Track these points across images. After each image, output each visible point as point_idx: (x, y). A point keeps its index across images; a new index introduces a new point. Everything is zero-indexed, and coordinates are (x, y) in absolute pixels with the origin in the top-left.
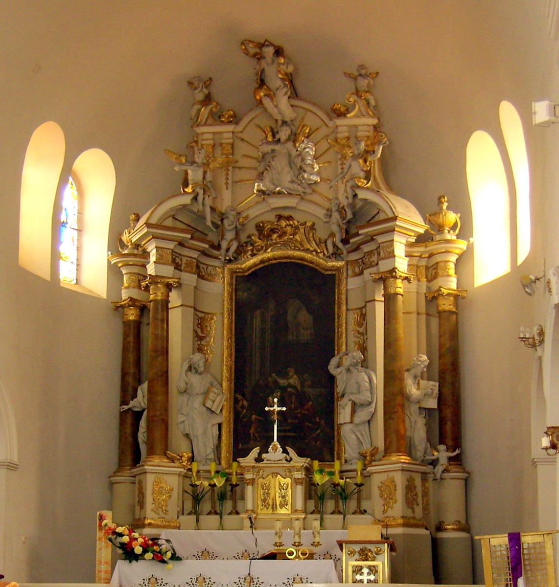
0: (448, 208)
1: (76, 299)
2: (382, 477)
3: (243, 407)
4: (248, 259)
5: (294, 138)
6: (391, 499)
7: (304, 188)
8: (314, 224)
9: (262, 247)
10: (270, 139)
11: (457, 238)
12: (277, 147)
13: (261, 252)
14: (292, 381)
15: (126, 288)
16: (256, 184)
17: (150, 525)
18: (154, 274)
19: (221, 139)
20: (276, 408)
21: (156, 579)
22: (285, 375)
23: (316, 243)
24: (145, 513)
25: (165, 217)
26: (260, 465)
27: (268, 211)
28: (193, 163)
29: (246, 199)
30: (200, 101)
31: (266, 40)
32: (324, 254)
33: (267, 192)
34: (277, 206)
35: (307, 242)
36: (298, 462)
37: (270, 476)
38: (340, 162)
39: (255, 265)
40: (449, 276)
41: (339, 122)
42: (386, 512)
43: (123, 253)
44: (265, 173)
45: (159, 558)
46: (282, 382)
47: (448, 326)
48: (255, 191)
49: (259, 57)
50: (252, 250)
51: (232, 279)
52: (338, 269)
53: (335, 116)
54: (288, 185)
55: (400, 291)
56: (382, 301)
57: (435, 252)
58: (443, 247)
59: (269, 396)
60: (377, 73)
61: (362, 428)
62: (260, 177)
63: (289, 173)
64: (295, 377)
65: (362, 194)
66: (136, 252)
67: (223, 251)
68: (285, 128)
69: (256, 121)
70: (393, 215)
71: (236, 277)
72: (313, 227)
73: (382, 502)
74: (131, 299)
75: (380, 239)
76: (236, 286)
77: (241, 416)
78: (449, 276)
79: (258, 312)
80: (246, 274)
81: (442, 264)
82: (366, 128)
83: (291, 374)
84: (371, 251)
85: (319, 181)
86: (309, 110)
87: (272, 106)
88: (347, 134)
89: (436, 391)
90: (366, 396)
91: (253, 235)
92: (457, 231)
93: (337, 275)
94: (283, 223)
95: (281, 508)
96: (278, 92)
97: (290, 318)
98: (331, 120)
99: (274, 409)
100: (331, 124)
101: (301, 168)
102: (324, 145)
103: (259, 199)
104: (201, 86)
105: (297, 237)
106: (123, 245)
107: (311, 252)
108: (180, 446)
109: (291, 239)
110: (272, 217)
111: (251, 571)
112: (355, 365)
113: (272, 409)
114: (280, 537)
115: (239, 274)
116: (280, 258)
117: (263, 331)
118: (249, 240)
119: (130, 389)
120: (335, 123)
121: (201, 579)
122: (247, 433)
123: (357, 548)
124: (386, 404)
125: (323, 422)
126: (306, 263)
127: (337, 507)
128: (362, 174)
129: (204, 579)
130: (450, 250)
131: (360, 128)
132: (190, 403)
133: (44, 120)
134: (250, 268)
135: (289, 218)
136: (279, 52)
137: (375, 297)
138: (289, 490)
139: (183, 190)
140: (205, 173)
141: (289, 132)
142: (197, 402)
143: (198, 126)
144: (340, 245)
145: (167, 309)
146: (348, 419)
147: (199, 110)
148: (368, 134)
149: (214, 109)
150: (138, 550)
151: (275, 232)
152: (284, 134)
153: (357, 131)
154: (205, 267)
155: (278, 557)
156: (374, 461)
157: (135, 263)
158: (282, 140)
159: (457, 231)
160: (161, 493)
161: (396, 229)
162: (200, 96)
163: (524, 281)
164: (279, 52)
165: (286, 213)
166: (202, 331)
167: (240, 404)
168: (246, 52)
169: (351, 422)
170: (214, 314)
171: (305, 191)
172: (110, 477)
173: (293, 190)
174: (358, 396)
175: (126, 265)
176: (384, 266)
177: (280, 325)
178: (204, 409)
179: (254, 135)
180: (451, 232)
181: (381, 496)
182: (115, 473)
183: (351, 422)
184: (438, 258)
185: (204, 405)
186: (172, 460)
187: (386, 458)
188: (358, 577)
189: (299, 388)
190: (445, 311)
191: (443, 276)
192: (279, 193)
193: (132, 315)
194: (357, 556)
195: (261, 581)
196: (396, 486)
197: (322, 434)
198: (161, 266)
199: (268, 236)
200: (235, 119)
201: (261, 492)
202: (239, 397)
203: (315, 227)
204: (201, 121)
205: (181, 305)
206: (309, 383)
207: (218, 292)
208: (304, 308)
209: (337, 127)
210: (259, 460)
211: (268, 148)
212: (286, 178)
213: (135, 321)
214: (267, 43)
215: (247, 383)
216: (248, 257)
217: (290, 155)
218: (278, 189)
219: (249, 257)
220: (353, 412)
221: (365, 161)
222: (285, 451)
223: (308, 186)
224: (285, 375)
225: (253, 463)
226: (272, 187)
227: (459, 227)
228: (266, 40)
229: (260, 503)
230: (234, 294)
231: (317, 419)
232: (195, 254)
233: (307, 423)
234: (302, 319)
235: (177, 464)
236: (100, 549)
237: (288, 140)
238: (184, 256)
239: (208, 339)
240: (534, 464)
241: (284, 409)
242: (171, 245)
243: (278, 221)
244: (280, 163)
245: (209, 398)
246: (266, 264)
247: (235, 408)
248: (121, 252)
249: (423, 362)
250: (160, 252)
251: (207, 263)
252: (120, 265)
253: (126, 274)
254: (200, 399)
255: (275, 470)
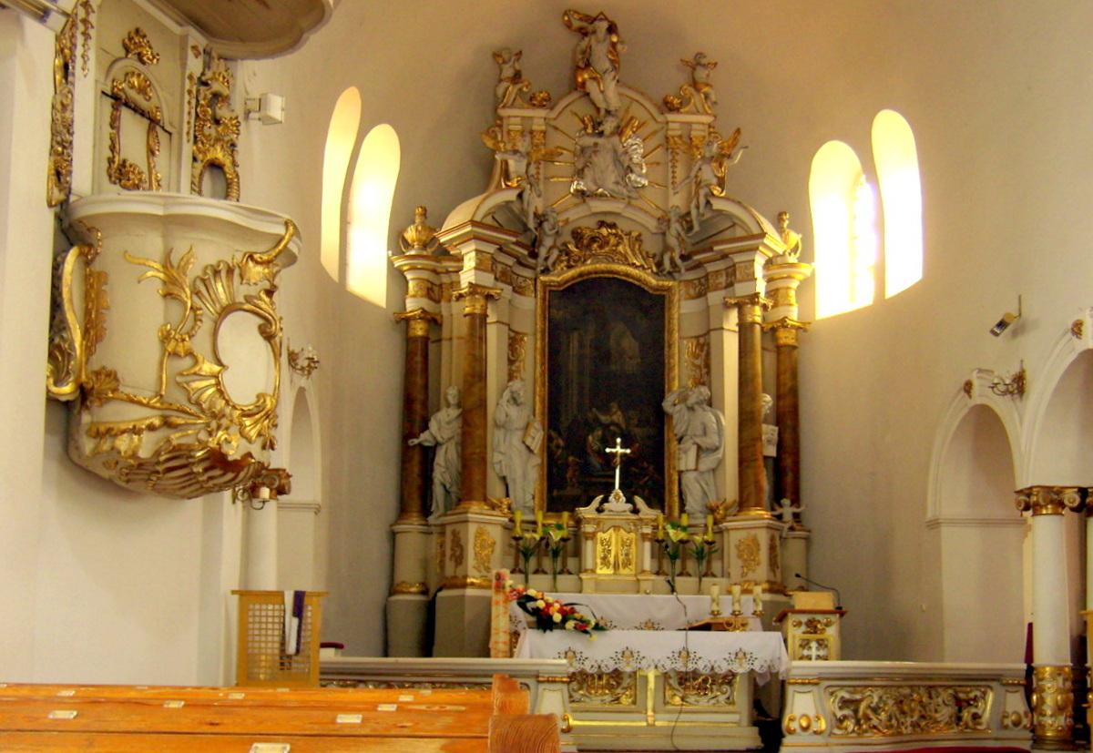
0: (789, 227)
1: (359, 303)
2: (743, 534)
3: (558, 447)
4: (562, 272)
5: (619, 131)
6: (754, 560)
7: (629, 191)
8: (640, 235)
9: (580, 258)
10: (590, 131)
11: (799, 261)
12: (600, 141)
13: (579, 264)
14: (615, 418)
15: (414, 296)
16: (575, 183)
17: (472, 584)
18: (474, 282)
19: (509, 125)
20: (619, 450)
21: (574, 653)
22: (607, 411)
23: (643, 257)
24: (466, 571)
25: (491, 213)
26: (602, 516)
27: (586, 216)
28: (515, 152)
29: (560, 198)
30: (508, 78)
31: (602, 13)
32: (652, 271)
33: (588, 193)
34: (598, 210)
35: (632, 257)
36: (647, 514)
37: (611, 531)
38: (670, 164)
39: (573, 278)
40: (791, 305)
41: (671, 117)
42: (746, 574)
43: (408, 254)
44: (586, 170)
45: (582, 627)
46: (604, 419)
47: (781, 367)
48: (572, 190)
49: (584, 33)
50: (568, 261)
51: (545, 293)
52: (669, 289)
53: (667, 109)
54: (612, 186)
55: (758, 319)
56: (734, 331)
57: (776, 276)
58: (784, 272)
59: (588, 435)
60: (716, 64)
61: (706, 476)
62: (580, 173)
63: (614, 172)
64: (619, 413)
65: (717, 205)
66: (425, 253)
67: (540, 260)
68: (610, 119)
69: (573, 108)
70: (759, 232)
71: (550, 291)
72: (639, 238)
73: (740, 563)
74: (424, 311)
75: (737, 258)
76: (549, 301)
77: (556, 457)
78: (791, 305)
79: (575, 335)
80: (562, 288)
81: (781, 291)
82: (701, 127)
83: (614, 410)
84: (717, 271)
85: (647, 184)
86: (637, 101)
87: (598, 91)
88: (679, 133)
89: (776, 437)
90: (712, 440)
91: (570, 243)
92: (798, 254)
93: (667, 297)
94: (604, 231)
95: (624, 568)
96: (606, 75)
97: (612, 343)
98: (662, 114)
99: (617, 452)
100: (660, 118)
101: (629, 167)
102: (653, 142)
103: (576, 201)
104: (513, 59)
105: (620, 248)
106: (408, 245)
107: (637, 267)
108: (495, 490)
109: (614, 251)
110: (592, 223)
111: (689, 641)
112: (699, 403)
113: (614, 450)
114: (718, 604)
115: (553, 288)
116: (603, 272)
117: (581, 358)
118: (564, 248)
119: (418, 419)
120: (666, 118)
121: (627, 653)
122: (571, 481)
123: (804, 618)
124: (741, 450)
125: (651, 468)
126: (631, 280)
127: (539, 564)
128: (714, 181)
129: (632, 653)
130: (793, 275)
131: (694, 126)
132: (508, 439)
133: (351, 85)
134: (567, 281)
135: (613, 226)
136: (612, 29)
137: (722, 324)
138: (633, 546)
139: (506, 185)
140: (529, 165)
141: (615, 124)
142: (516, 439)
143: (504, 107)
144: (679, 262)
145: (486, 324)
146: (692, 465)
147: (507, 89)
148: (703, 134)
149: (525, 89)
150: (557, 617)
151: (595, 241)
152: (608, 126)
153: (691, 130)
154: (515, 277)
155: (713, 627)
156: (730, 516)
157: (425, 267)
158: (607, 132)
159: (798, 254)
160: (483, 547)
161: (761, 248)
162: (508, 72)
163: (894, 322)
164: (612, 29)
165: (609, 220)
166: (513, 355)
167: (555, 442)
168: (569, 25)
169: (696, 470)
170: (525, 334)
171: (630, 195)
172: (391, 526)
173: (617, 193)
174: (704, 439)
175: (413, 268)
176: (741, 290)
177: (603, 355)
178: (523, 448)
179: (570, 123)
180: (792, 254)
181: (740, 556)
182: (396, 523)
183: (696, 470)
184: (779, 284)
185: (524, 442)
186: (493, 507)
187: (740, 514)
188: (806, 652)
189: (624, 426)
190: (785, 346)
191: (782, 305)
192: (602, 195)
193: (419, 329)
194: (803, 628)
195: (641, 655)
196: (759, 545)
197: (650, 483)
198: (480, 273)
199: (589, 246)
200: (547, 103)
201: (599, 548)
202: (553, 434)
203: (643, 237)
204: (507, 102)
205: (497, 322)
206: (636, 422)
207: (529, 308)
208: (628, 333)
209: (667, 123)
210: (599, 510)
211: (589, 141)
212: (611, 177)
213: (422, 337)
214: (602, 16)
215: (563, 419)
216: (562, 269)
217: (615, 151)
218: (600, 190)
219: (565, 269)
220: (698, 457)
221: (721, 166)
222: (629, 500)
223: (638, 192)
224: (607, 411)
225: (595, 515)
226: (594, 188)
227: (800, 249)
228: (602, 13)
229: (599, 561)
230: (547, 313)
231: (645, 465)
232: (510, 261)
233: (634, 469)
234: (627, 344)
235: (496, 512)
236: (498, 616)
237: (612, 134)
238: (500, 262)
239: (517, 364)
240: (935, 524)
241: (628, 451)
242: (491, 249)
243: (599, 228)
244: (603, 161)
245: (529, 435)
246: (585, 277)
247: (549, 447)
248: (404, 253)
249: (768, 403)
250: (480, 256)
251: (518, 273)
252: (405, 268)
253: (413, 279)
254: (520, 433)
255: (617, 523)
